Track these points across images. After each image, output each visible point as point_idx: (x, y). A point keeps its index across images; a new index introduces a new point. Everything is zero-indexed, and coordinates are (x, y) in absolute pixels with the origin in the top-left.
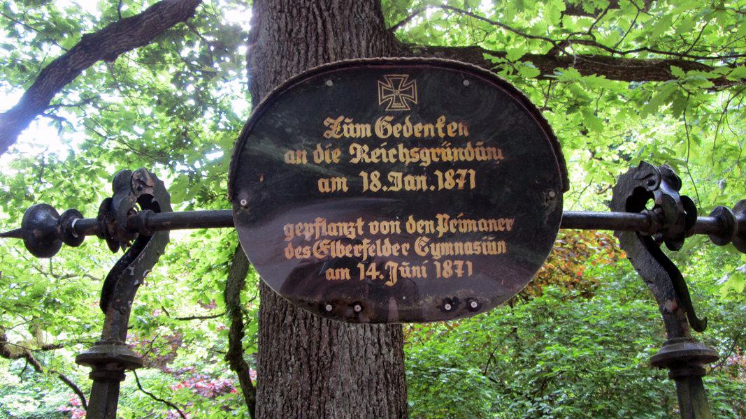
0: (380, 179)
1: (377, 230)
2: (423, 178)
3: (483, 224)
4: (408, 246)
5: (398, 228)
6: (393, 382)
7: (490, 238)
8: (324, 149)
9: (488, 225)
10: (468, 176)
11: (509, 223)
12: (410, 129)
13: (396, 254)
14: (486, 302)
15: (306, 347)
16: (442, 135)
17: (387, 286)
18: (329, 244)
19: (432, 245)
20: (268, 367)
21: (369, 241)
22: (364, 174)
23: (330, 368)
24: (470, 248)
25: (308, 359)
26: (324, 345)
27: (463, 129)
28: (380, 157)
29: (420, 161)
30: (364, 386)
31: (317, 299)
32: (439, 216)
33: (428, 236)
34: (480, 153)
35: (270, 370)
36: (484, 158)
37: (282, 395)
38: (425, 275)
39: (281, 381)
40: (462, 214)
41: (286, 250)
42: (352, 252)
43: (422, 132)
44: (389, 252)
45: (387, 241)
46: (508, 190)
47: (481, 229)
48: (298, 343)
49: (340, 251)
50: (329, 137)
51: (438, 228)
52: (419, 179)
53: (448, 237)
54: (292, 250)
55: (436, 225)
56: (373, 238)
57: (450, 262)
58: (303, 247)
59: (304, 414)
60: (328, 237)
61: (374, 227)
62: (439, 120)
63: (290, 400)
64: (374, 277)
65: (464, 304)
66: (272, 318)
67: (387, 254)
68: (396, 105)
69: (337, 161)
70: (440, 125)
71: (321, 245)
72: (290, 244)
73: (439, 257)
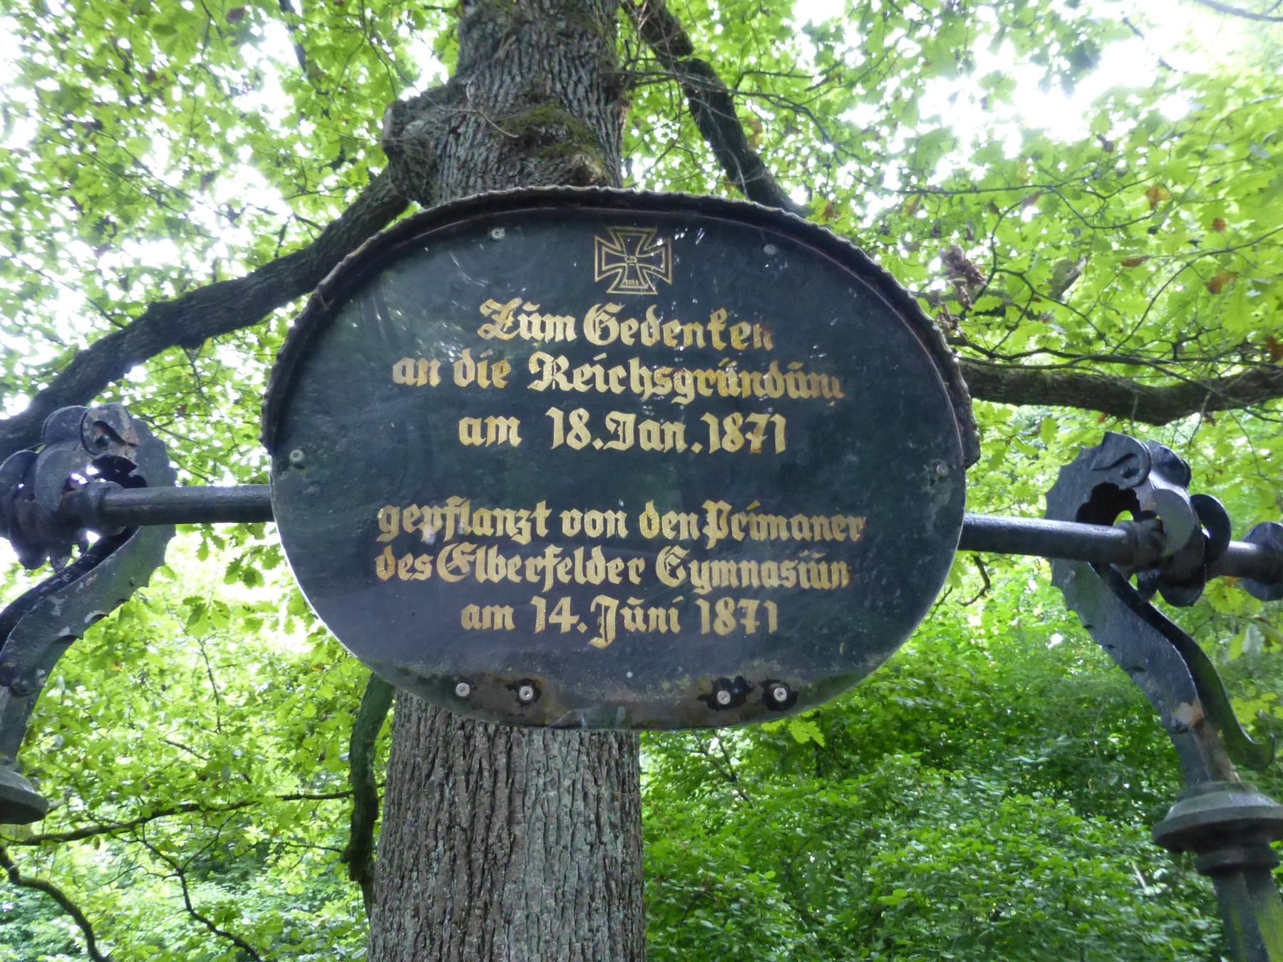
0: (588, 425)
1: (578, 527)
2: (679, 428)
3: (800, 524)
4: (642, 564)
5: (622, 525)
6: (621, 897)
7: (817, 555)
8: (477, 360)
9: (812, 528)
10: (771, 427)
11: (855, 526)
12: (651, 330)
13: (615, 580)
14: (807, 689)
15: (465, 825)
16: (718, 344)
17: (594, 649)
18: (473, 552)
19: (694, 566)
20: (396, 862)
21: (558, 550)
22: (555, 413)
23: (506, 865)
24: (774, 574)
25: (469, 848)
26: (499, 821)
27: (762, 335)
28: (592, 380)
29: (674, 393)
30: (570, 903)
31: (442, 669)
32: (711, 507)
33: (683, 545)
35: (399, 867)
36: (804, 393)
37: (416, 914)
38: (676, 628)
39: (417, 887)
40: (756, 504)
41: (380, 561)
42: (521, 571)
43: (680, 338)
44: (602, 576)
45: (597, 552)
46: (852, 458)
47: (797, 536)
48: (452, 818)
49: (495, 568)
50: (490, 336)
51: (705, 530)
52: (669, 428)
53: (728, 549)
54: (391, 560)
55: (702, 523)
56: (569, 545)
57: (731, 602)
58: (415, 557)
59: (454, 952)
60: (472, 538)
61: (571, 522)
62: (713, 317)
63: (430, 926)
64: (566, 628)
65: (760, 691)
66: (409, 769)
67: (597, 580)
68: (628, 284)
69: (500, 383)
70: (715, 326)
71: (455, 555)
72: (388, 550)
73: (708, 589)
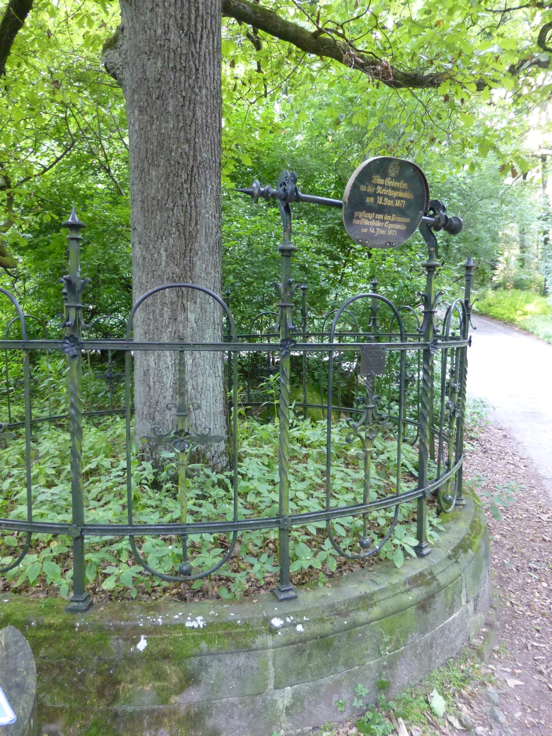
24: (398, 227)
34: (407, 195)
37: (166, 250)
49: (367, 223)
53: (394, 222)
